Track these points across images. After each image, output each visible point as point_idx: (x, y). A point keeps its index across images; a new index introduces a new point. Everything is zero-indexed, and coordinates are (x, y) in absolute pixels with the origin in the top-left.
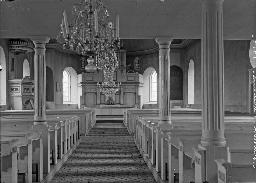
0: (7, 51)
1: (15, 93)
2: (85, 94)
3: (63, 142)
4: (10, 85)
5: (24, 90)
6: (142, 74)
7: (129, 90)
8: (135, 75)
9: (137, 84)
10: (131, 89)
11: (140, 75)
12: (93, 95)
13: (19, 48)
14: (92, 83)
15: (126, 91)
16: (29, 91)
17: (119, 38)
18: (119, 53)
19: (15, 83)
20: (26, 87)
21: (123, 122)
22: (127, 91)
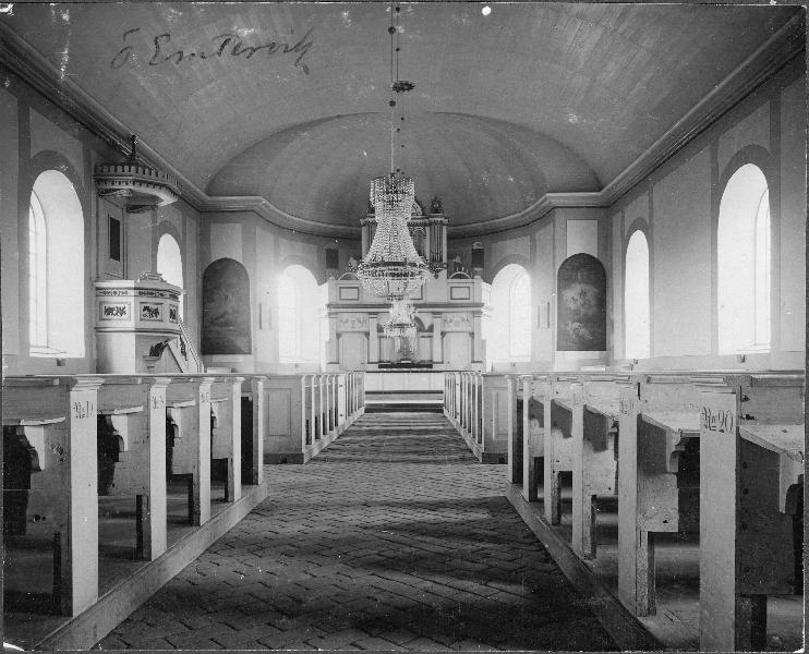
0: (93, 195)
1: (115, 322)
2: (338, 336)
3: (307, 421)
4: (101, 299)
9: (476, 308)
11: (485, 285)
12: (359, 340)
13: (127, 187)
17: (324, 370)
18: (430, 224)
19: (115, 293)
21: (442, 411)
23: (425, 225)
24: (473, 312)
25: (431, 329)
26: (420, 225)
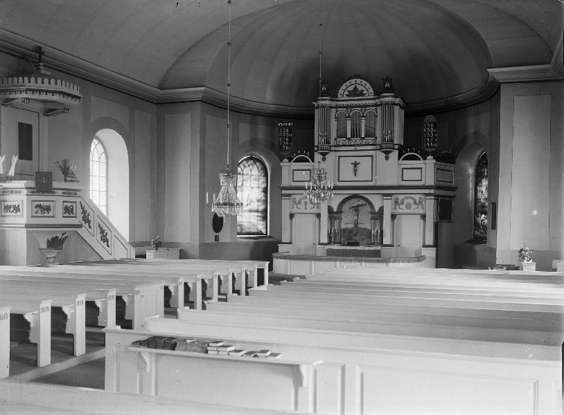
5: (36, 210)
10: (412, 203)
16: (51, 214)
19: (12, 192)
20: (42, 203)
22: (402, 209)
23: (376, 105)
26: (344, 107)
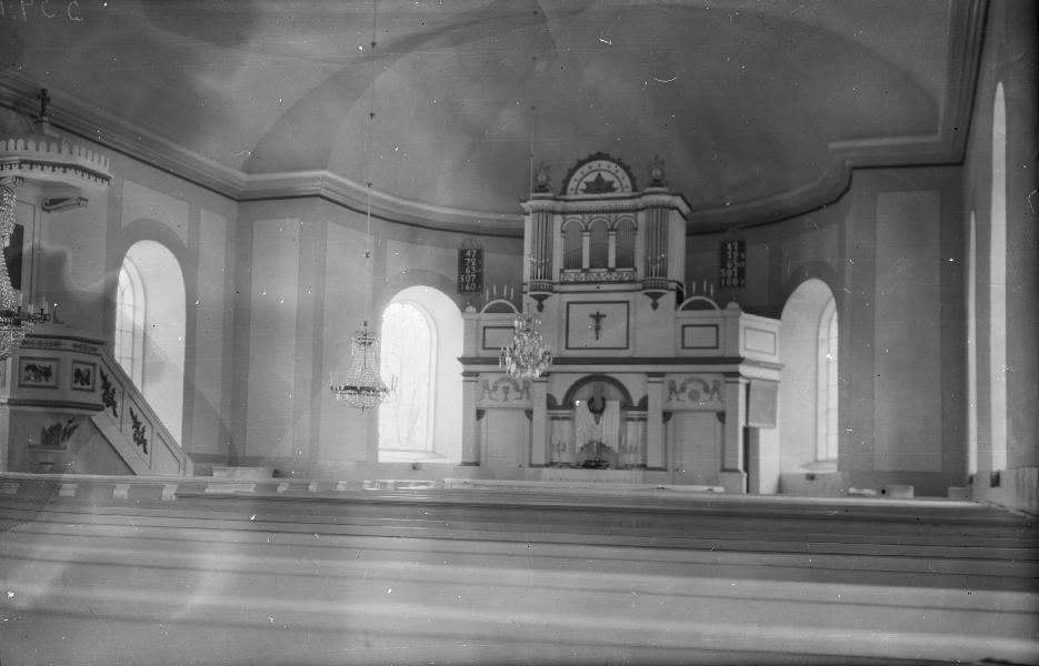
2: (480, 414)
6: (775, 313)
7: (694, 396)
8: (719, 321)
14: (479, 363)
15: (679, 400)
20: (37, 363)
24: (727, 374)
25: (644, 404)
